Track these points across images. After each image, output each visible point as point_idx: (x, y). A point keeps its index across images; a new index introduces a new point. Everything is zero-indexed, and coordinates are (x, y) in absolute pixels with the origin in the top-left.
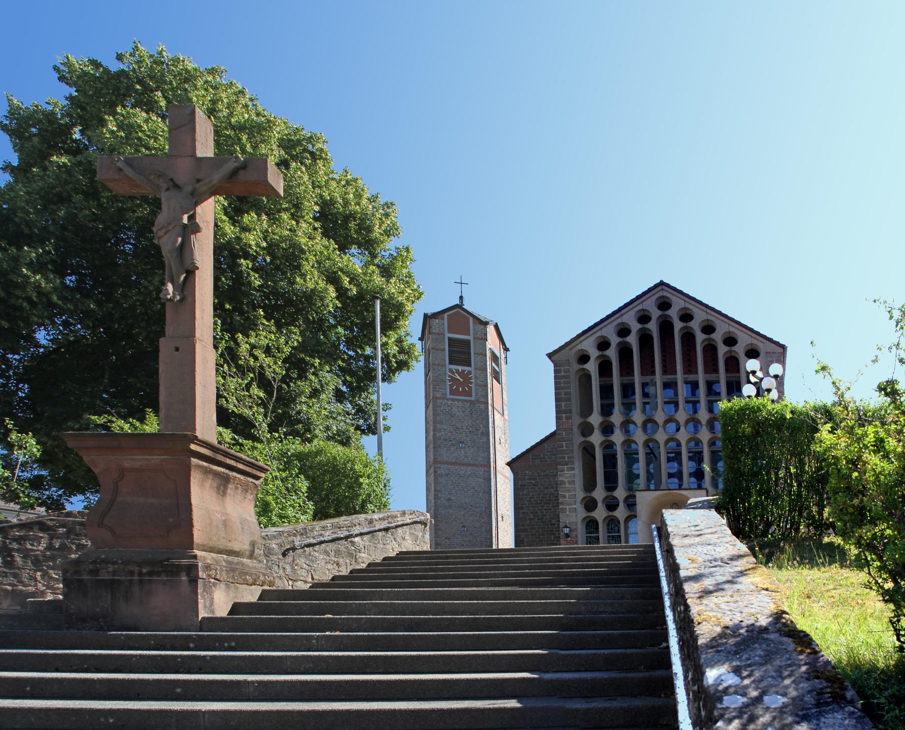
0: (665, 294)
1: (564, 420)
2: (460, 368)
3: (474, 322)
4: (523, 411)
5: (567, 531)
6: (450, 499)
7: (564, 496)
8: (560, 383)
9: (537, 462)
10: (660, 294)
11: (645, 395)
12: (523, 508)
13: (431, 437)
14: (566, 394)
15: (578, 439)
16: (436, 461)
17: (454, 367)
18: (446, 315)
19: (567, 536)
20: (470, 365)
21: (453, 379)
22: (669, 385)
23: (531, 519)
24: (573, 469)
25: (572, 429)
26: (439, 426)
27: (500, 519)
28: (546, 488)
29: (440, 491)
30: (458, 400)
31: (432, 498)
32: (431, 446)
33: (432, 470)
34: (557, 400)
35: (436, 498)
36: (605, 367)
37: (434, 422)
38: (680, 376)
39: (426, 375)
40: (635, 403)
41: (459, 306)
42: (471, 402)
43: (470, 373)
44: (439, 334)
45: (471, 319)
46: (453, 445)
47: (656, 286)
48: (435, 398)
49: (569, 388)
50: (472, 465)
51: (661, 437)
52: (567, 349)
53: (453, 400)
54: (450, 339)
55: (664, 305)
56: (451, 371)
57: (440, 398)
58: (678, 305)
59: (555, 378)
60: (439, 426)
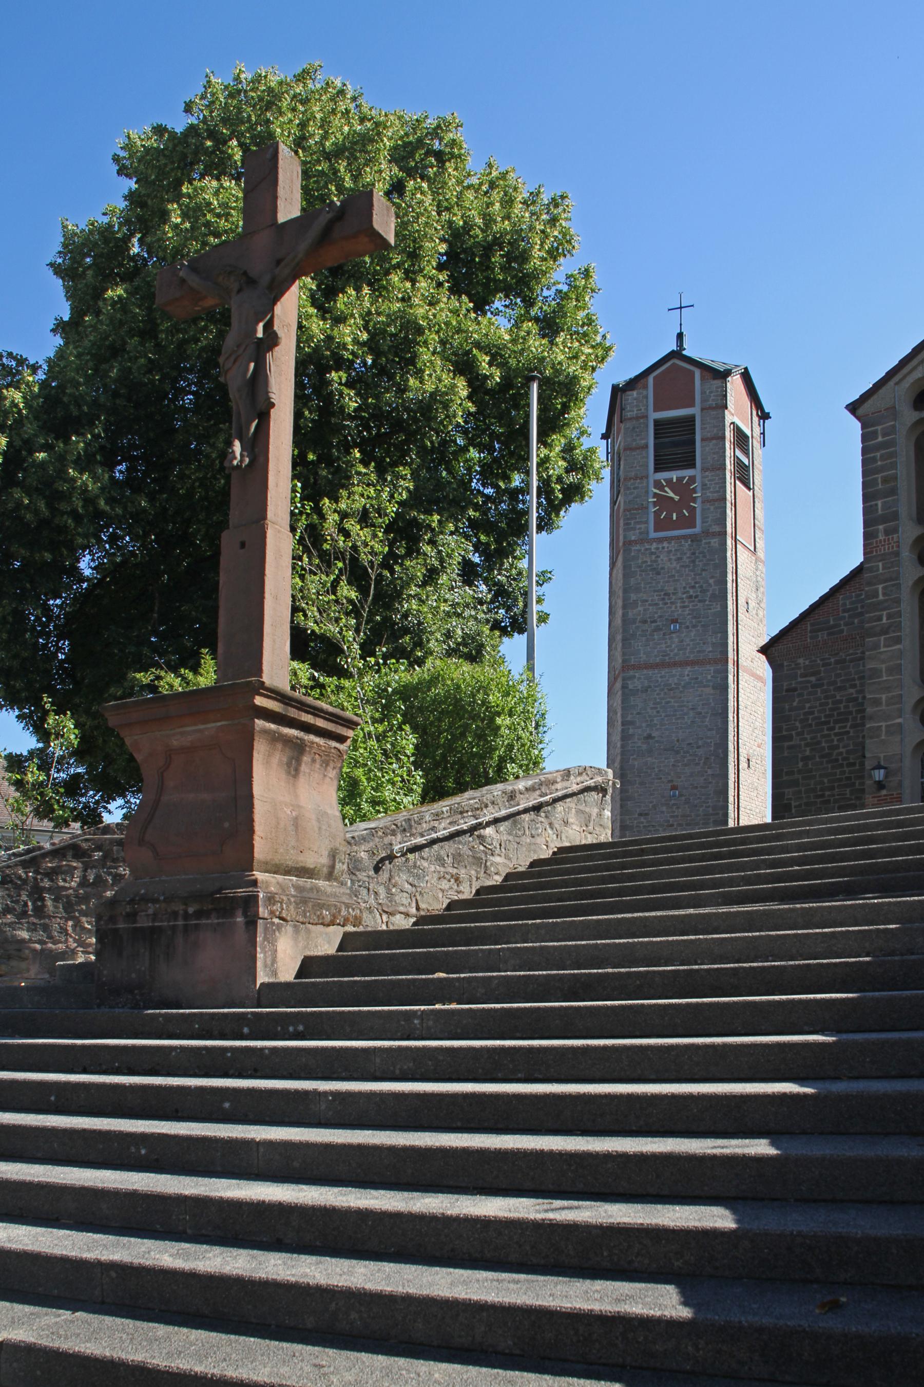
1: (881, 537)
3: (703, 378)
5: (879, 775)
6: (649, 737)
7: (877, 702)
9: (822, 636)
12: (790, 738)
13: (618, 621)
16: (626, 666)
24: (898, 640)
26: (633, 597)
27: (743, 764)
28: (840, 689)
29: (632, 723)
30: (669, 539)
31: (617, 737)
32: (619, 637)
33: (618, 685)
35: (625, 737)
37: (625, 591)
39: (613, 502)
41: (677, 354)
42: (694, 538)
44: (637, 418)
45: (697, 373)
46: (658, 629)
48: (628, 543)
50: (693, 663)
53: (660, 540)
60: (633, 597)
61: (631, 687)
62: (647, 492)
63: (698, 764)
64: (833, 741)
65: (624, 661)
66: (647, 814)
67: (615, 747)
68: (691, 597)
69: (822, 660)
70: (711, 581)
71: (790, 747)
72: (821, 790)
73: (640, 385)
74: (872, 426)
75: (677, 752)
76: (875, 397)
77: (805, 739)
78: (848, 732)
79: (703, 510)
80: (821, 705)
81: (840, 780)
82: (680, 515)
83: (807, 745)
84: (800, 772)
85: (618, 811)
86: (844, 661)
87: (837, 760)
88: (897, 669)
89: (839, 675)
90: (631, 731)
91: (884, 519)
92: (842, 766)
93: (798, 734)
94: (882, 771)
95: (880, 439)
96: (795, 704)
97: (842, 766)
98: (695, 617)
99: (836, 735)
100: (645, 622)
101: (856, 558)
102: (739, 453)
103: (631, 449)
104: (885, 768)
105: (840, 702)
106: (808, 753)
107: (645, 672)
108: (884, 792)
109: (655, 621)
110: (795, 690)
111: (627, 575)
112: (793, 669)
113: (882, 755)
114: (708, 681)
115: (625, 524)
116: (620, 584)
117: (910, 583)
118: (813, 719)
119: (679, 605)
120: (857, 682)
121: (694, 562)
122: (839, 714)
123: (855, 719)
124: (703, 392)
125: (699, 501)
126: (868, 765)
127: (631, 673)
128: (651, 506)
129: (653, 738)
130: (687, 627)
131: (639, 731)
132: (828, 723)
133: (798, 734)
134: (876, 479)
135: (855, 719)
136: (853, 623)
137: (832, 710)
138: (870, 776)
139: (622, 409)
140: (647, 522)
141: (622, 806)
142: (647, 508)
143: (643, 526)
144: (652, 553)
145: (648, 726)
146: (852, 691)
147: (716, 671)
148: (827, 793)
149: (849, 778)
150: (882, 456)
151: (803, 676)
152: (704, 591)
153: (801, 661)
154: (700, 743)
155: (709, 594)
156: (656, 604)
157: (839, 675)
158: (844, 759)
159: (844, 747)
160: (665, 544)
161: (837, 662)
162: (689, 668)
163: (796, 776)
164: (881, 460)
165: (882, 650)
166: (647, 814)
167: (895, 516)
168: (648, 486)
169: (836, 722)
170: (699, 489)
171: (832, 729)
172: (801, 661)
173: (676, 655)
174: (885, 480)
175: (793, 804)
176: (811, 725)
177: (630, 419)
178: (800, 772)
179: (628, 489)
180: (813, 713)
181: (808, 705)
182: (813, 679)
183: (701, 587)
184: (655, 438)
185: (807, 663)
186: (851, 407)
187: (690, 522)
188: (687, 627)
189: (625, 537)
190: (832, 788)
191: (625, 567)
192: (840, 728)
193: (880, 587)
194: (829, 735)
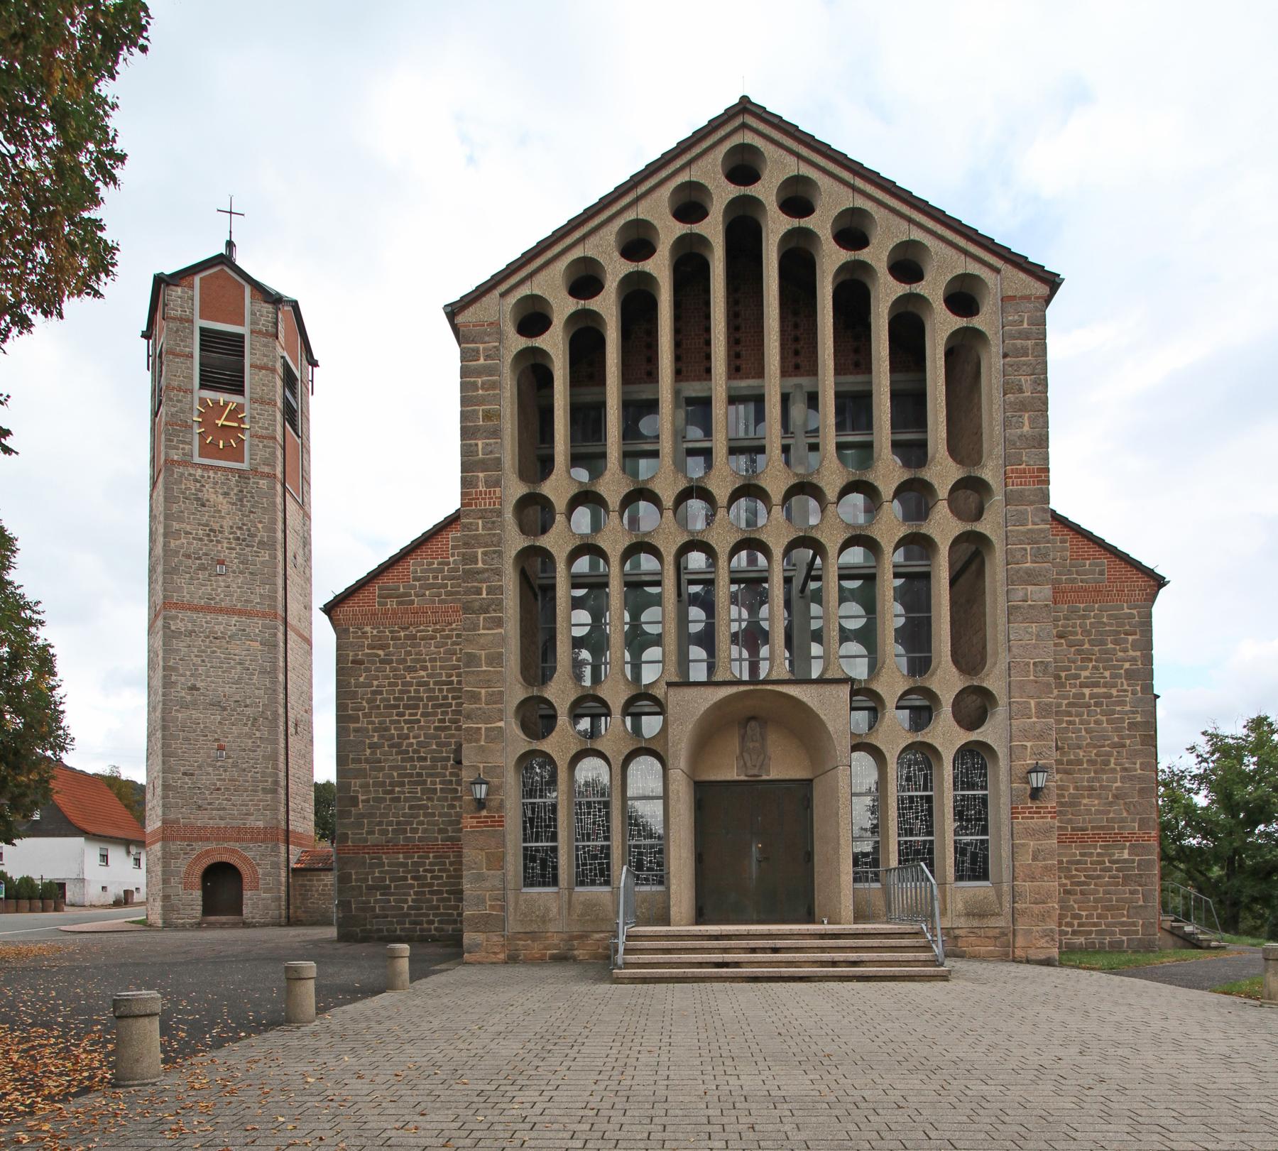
0: (749, 138)
1: (481, 488)
2: (222, 397)
3: (252, 297)
4: (385, 460)
5: (481, 791)
6: (194, 688)
7: (475, 697)
8: (474, 386)
9: (392, 604)
10: (736, 140)
11: (630, 431)
12: (357, 720)
13: (159, 550)
14: (488, 416)
15: (515, 541)
16: (167, 604)
17: (209, 395)
18: (197, 280)
19: (481, 804)
20: (241, 393)
21: (207, 421)
22: (699, 409)
23: (373, 746)
24: (499, 623)
25: (500, 513)
26: (176, 526)
27: (291, 730)
28: (410, 669)
29: (174, 669)
30: (216, 469)
31: (158, 682)
32: (160, 569)
33: (160, 623)
34: (466, 433)
35: (167, 684)
36: (586, 340)
37: (167, 517)
38: (719, 384)
39: (155, 413)
40: (603, 455)
41: (224, 260)
42: (241, 474)
43: (240, 408)
44: (181, 320)
45: (248, 290)
46: (202, 568)
47: (730, 114)
48: (170, 463)
49: (497, 399)
50: (240, 613)
51: (556, 542)
52: (496, 292)
53: (206, 468)
54: (202, 330)
55: (743, 169)
56: (203, 402)
57: (179, 463)
58: (779, 168)
59: (465, 372)
60: (176, 526)
61: (173, 628)
62: (192, 409)
63: (246, 725)
64: (402, 728)
65: (165, 597)
66: (192, 775)
67: (156, 694)
68: (238, 539)
69: (391, 632)
70: (260, 526)
71: (357, 730)
72: (391, 784)
73: (184, 283)
74: (473, 342)
75: (224, 709)
76: (477, 305)
77: (373, 723)
78: (419, 721)
79: (251, 445)
80: (390, 684)
81: (411, 775)
82: (228, 446)
83: (375, 730)
84: (367, 761)
85: (158, 767)
86: (414, 637)
87: (408, 752)
88: (496, 659)
89: (409, 653)
90: (174, 678)
91: (484, 465)
92: (412, 759)
93: (365, 715)
94: (484, 787)
95: (482, 361)
96: (361, 679)
97: (412, 759)
98: (242, 563)
99: (406, 722)
100: (188, 557)
101: (451, 502)
102: (288, 394)
103: (174, 354)
104: (487, 783)
105: (411, 684)
106: (376, 740)
107: (189, 613)
108: (484, 813)
109: (199, 558)
110: (361, 662)
111: (169, 499)
112: (359, 637)
113: (481, 766)
114: (256, 635)
115: (168, 440)
116: (161, 509)
117: (514, 553)
118: (381, 700)
119: (225, 545)
120: (428, 664)
121: (241, 500)
122: (409, 698)
123: (426, 706)
124: (253, 313)
125: (247, 433)
126: (466, 776)
127: (174, 612)
128: (195, 425)
129: (198, 689)
130: (234, 572)
131: (183, 679)
132: (397, 707)
133: (365, 715)
134: (476, 412)
135: (426, 706)
136: (424, 595)
137: (401, 692)
138: (470, 792)
139: (165, 305)
140: (190, 444)
141: (164, 762)
142: (191, 427)
143: (187, 447)
144: (196, 481)
145: (192, 675)
146: (423, 673)
147: (264, 626)
148: (397, 789)
149: (420, 775)
150: (483, 383)
151: (371, 647)
152: (252, 536)
153: (368, 629)
154: (248, 701)
155: (257, 540)
156: (201, 540)
157: (409, 653)
158: (415, 751)
159: (414, 737)
160: (211, 474)
161: (407, 637)
162: (236, 618)
163: (364, 765)
164: (483, 388)
165: (482, 632)
166: (192, 775)
167: (497, 465)
168: (192, 402)
169: (407, 707)
170: (247, 420)
171: (403, 715)
172: (368, 629)
173: (221, 600)
174: (488, 416)
175: (361, 798)
176: (378, 707)
177: (174, 319)
178: (367, 761)
179: (171, 400)
180: (381, 693)
181: (375, 683)
182: (381, 652)
183: (249, 530)
184: (201, 350)
185: (375, 632)
186: (449, 309)
187: (237, 455)
188: (234, 572)
189: (167, 454)
190: (402, 784)
191: (166, 489)
192: (411, 715)
193: (480, 551)
194: (399, 722)
